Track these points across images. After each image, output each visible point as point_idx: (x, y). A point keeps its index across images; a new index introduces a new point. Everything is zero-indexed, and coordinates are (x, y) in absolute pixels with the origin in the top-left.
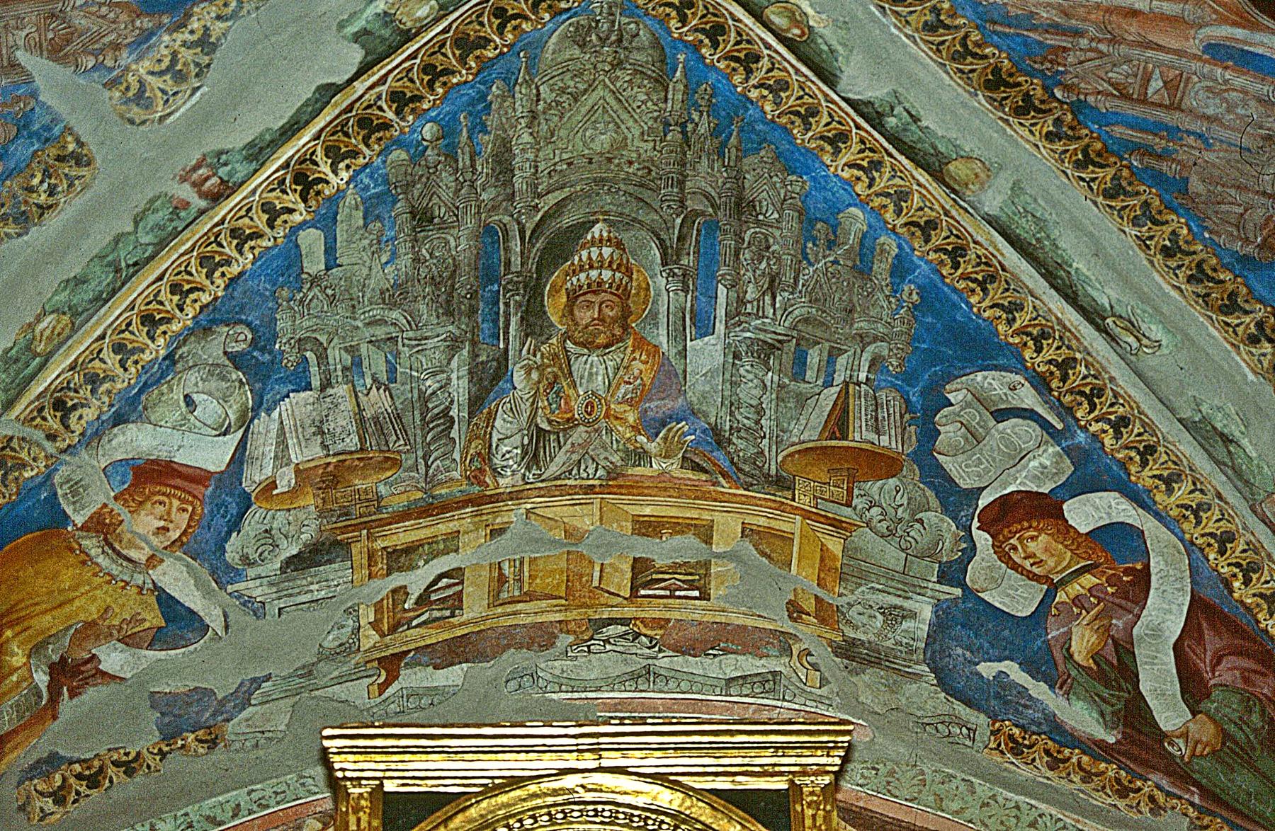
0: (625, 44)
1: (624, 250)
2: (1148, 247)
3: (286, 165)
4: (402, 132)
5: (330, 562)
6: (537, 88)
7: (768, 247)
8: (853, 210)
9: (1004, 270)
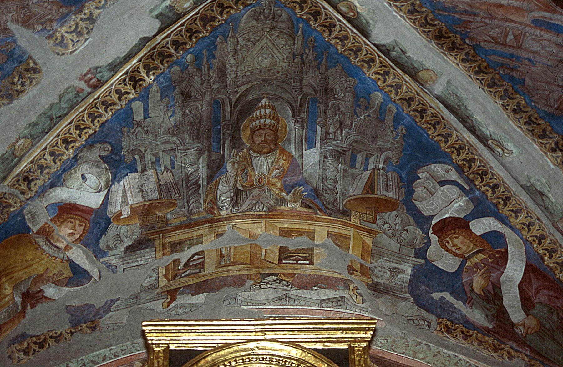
0: (276, 19)
1: (275, 110)
2: (507, 109)
3: (126, 73)
4: (178, 58)
5: (146, 248)
6: (237, 39)
7: (339, 109)
8: (377, 93)
9: (443, 119)
